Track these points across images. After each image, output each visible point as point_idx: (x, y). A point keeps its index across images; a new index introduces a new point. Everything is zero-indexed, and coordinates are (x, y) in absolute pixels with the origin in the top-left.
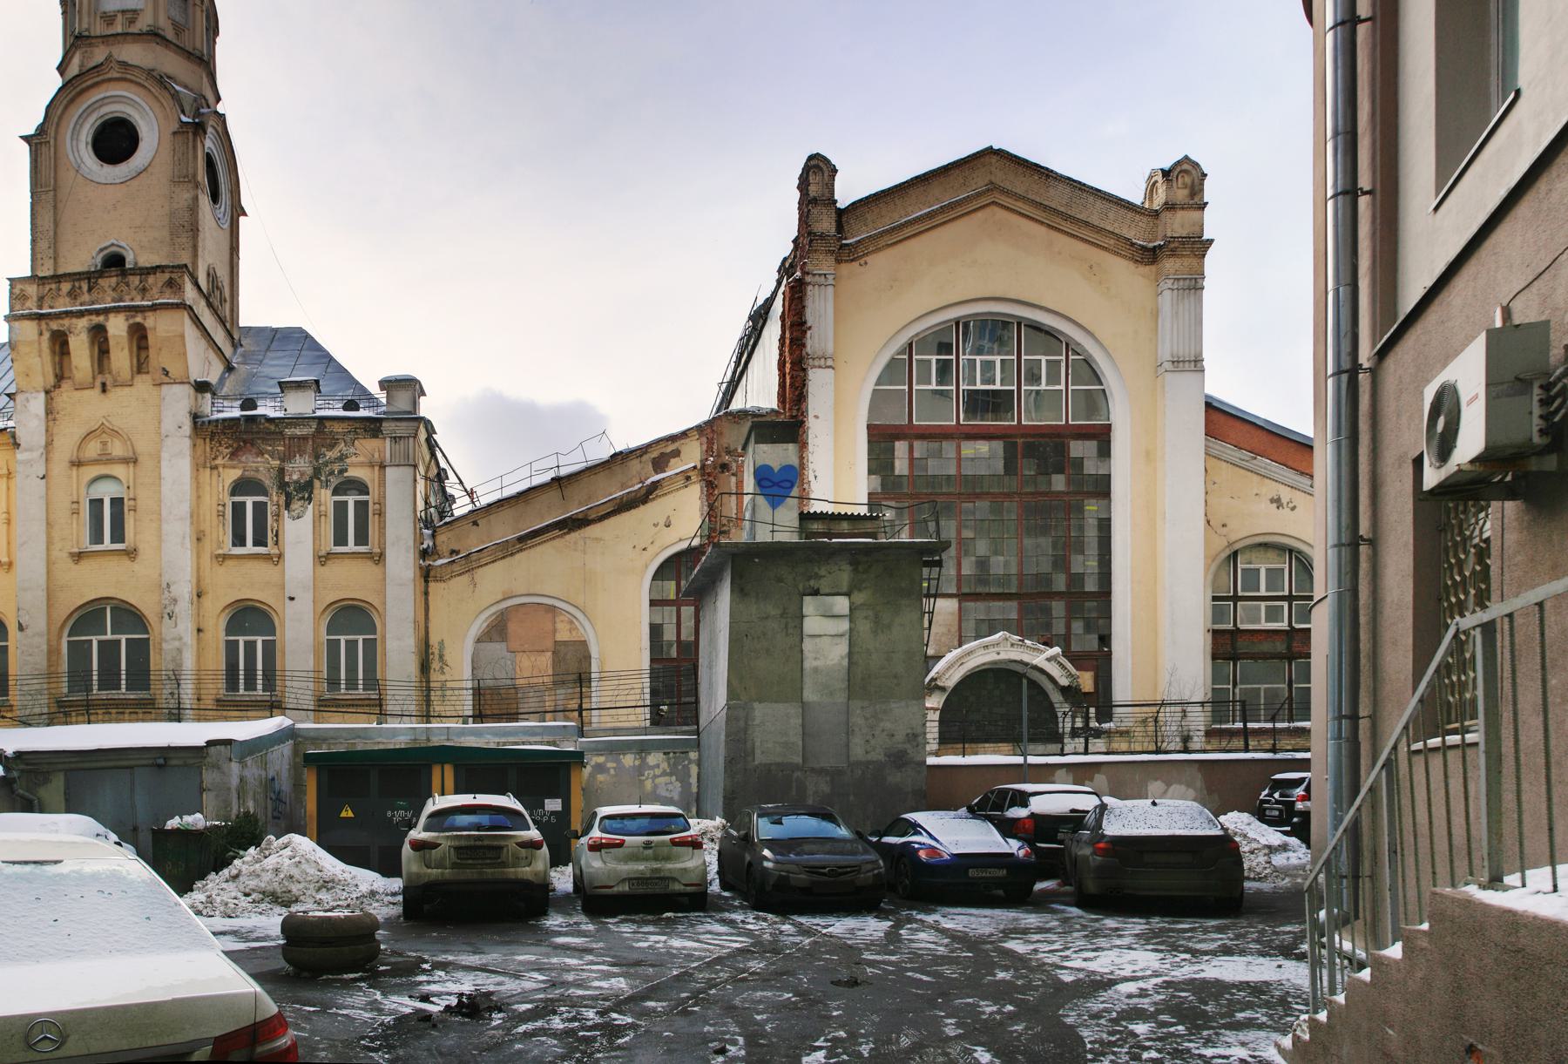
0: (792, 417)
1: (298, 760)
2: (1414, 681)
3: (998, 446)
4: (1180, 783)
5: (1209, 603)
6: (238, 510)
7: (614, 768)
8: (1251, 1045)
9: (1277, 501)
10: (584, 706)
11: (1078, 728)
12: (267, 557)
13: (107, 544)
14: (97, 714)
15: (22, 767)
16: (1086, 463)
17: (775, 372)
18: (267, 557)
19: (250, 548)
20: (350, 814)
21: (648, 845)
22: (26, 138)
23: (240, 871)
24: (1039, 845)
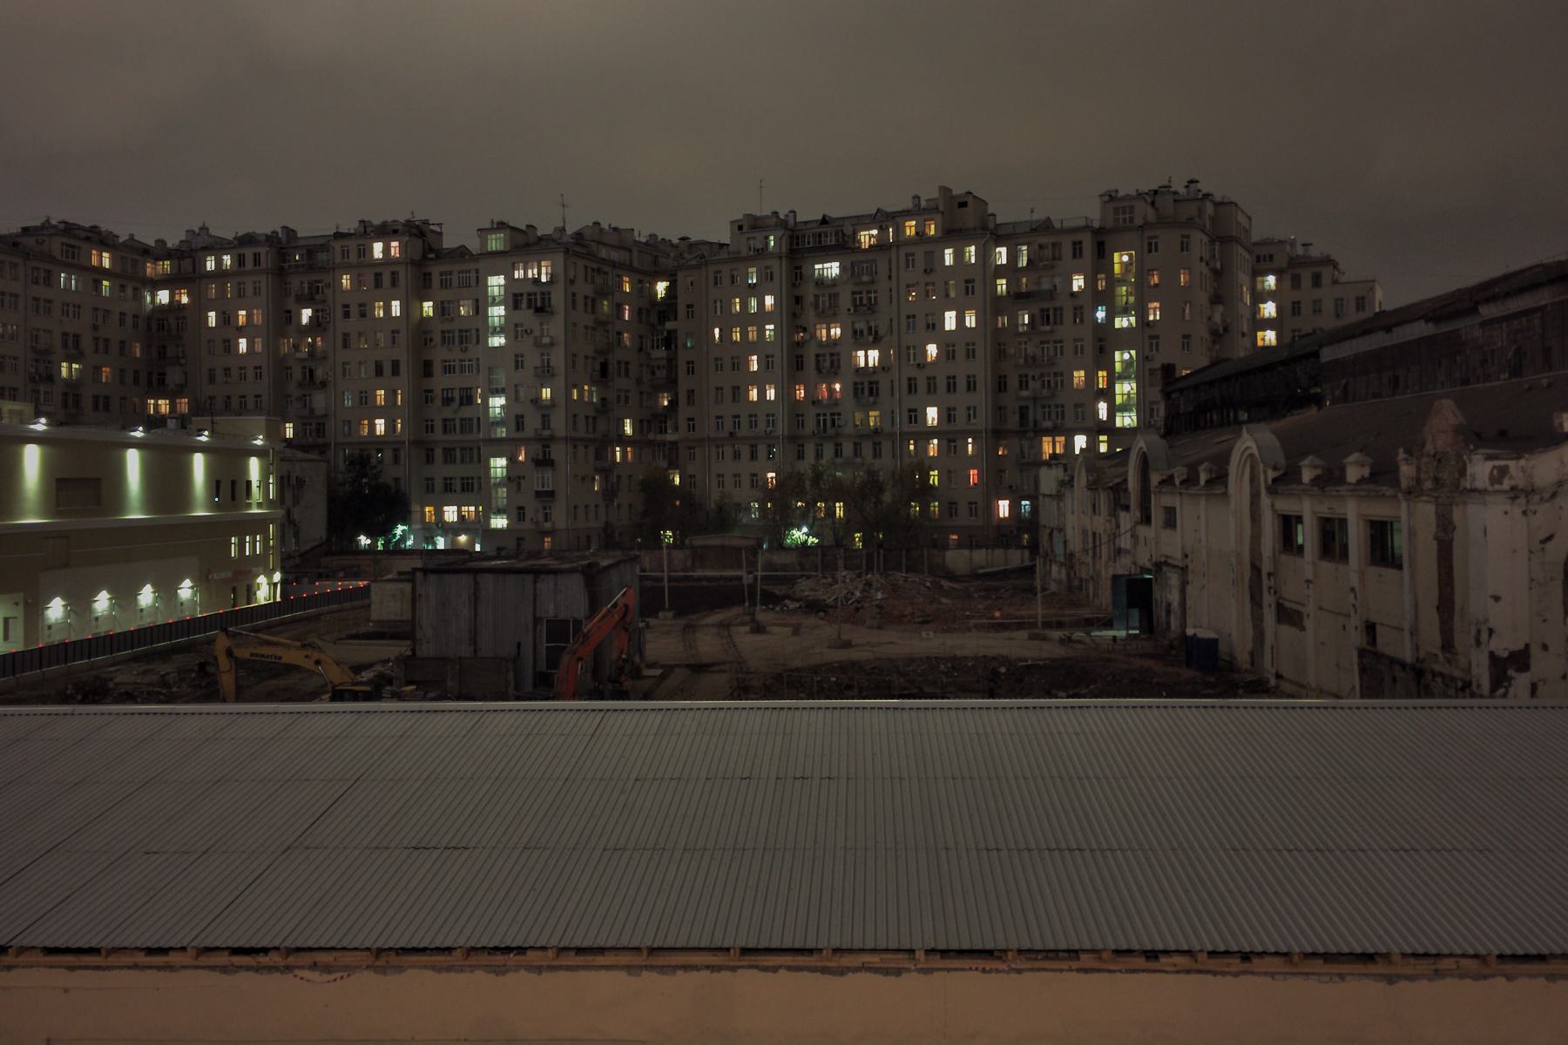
0: (767, 277)
2: (675, 297)
5: (1389, 520)
6: (967, 287)
7: (12, 326)
12: (446, 361)
13: (1153, 241)
15: (733, 539)
16: (549, 610)
18: (446, 361)
19: (1154, 253)
23: (626, 606)
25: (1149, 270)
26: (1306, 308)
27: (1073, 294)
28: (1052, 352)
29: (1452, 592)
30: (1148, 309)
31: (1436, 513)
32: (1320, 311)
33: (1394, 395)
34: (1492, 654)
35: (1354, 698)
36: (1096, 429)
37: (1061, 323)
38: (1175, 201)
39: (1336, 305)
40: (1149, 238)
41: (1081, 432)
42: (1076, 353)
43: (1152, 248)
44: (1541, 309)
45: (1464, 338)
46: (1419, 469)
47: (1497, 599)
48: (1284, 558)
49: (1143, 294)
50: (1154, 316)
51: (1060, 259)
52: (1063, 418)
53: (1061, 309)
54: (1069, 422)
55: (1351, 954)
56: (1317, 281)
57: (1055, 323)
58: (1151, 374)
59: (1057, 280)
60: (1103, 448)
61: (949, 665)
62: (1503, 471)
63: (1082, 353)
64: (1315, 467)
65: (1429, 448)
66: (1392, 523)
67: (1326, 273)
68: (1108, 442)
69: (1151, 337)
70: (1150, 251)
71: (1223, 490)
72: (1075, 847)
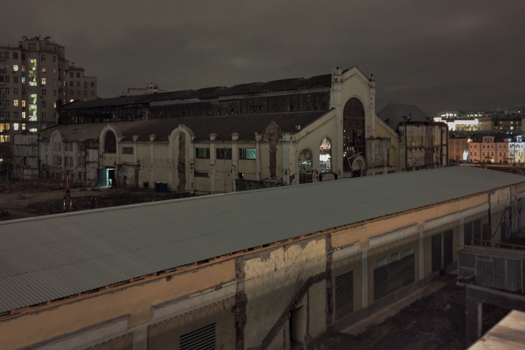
1: (267, 91)
3: (247, 158)
4: (325, 272)
8: (490, 154)
9: (235, 175)
10: (24, 144)
11: (121, 120)
13: (44, 57)
14: (104, 196)
17: (349, 271)
19: (44, 61)
20: (502, 128)
21: (203, 292)
22: (85, 71)
24: (64, 93)
25: (42, 67)
26: (75, 84)
27: (14, 72)
28: (4, 92)
29: (275, 164)
30: (42, 80)
31: (270, 147)
32: (79, 85)
33: (183, 117)
34: (290, 176)
35: (234, 192)
36: (21, 121)
37: (8, 82)
38: (46, 43)
39: (85, 84)
40: (42, 55)
41: (17, 122)
42: (15, 93)
43: (43, 59)
44: (240, 99)
45: (212, 104)
46: (263, 137)
47: (291, 164)
48: (197, 160)
49: (39, 75)
50: (44, 83)
51: (8, 58)
52: (9, 117)
53: (8, 77)
54: (12, 117)
55: (93, 290)
56: (78, 75)
57: (6, 82)
58: (42, 103)
59: (7, 66)
60: (24, 128)
61: (77, 200)
62: (291, 137)
63: (17, 93)
64: (215, 136)
65: (267, 132)
66: (245, 149)
67: (81, 73)
68: (26, 126)
69: (43, 90)
70: (42, 60)
71: (167, 142)
72: (24, 272)
